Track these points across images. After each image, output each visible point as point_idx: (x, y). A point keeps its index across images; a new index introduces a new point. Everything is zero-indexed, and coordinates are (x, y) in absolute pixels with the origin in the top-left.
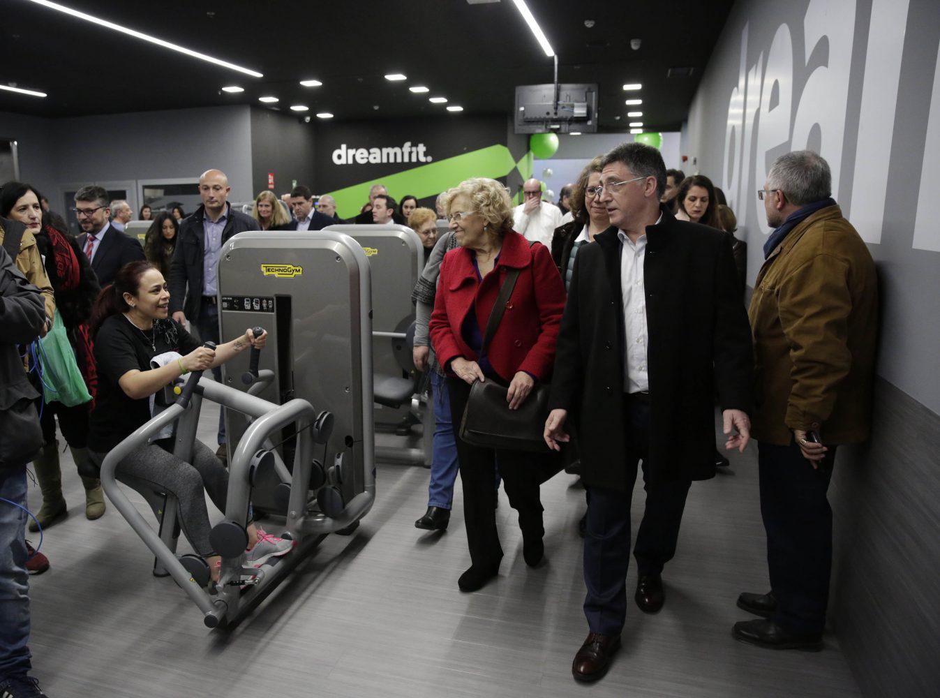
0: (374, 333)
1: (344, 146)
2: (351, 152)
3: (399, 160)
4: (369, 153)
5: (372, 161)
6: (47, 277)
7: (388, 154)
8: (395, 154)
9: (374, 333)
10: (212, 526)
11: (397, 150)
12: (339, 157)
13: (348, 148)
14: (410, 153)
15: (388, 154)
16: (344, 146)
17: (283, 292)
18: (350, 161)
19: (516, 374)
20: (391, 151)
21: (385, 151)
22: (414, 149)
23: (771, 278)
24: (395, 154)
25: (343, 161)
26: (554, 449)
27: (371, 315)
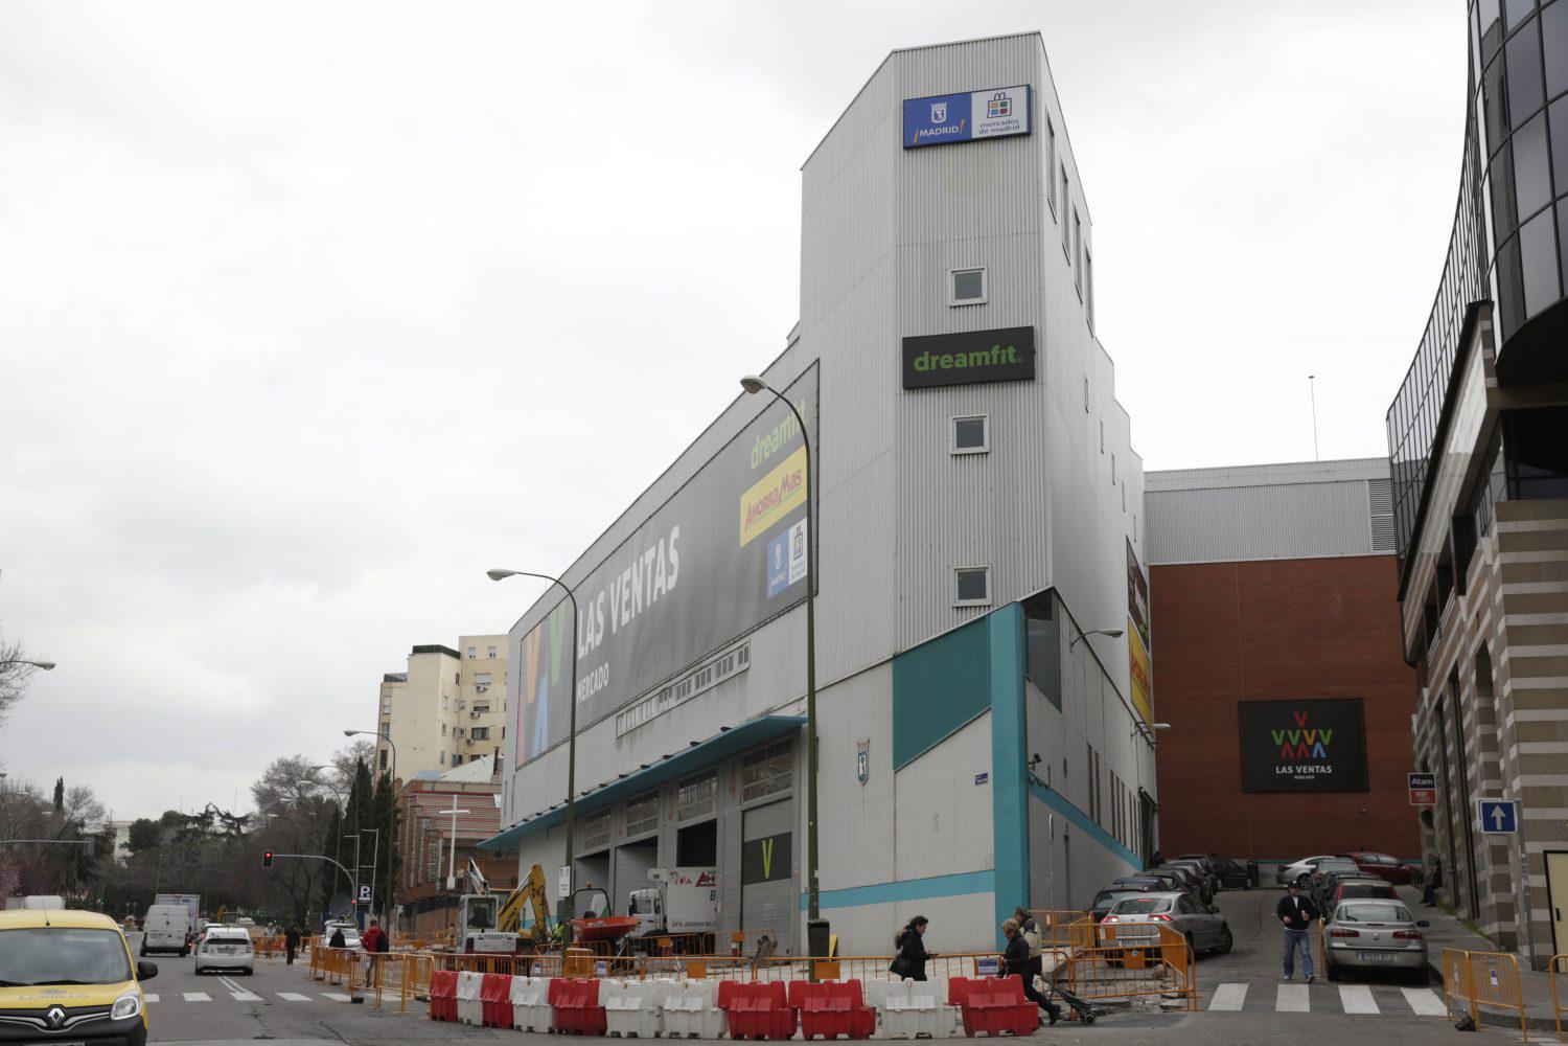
0: (767, 876)
1: (926, 354)
2: (934, 359)
3: (987, 362)
4: (955, 359)
5: (957, 365)
6: (832, 939)
7: (975, 358)
8: (983, 358)
9: (767, 876)
10: (742, 544)
11: (986, 354)
12: (922, 364)
13: (930, 355)
14: (999, 356)
15: (975, 358)
16: (926, 354)
17: (1053, 355)
18: (934, 367)
19: (922, 939)
20: (979, 355)
21: (972, 355)
22: (1003, 351)
23: (1453, 476)
24: (983, 358)
25: (926, 367)
26: (367, 766)
27: (263, 1038)
